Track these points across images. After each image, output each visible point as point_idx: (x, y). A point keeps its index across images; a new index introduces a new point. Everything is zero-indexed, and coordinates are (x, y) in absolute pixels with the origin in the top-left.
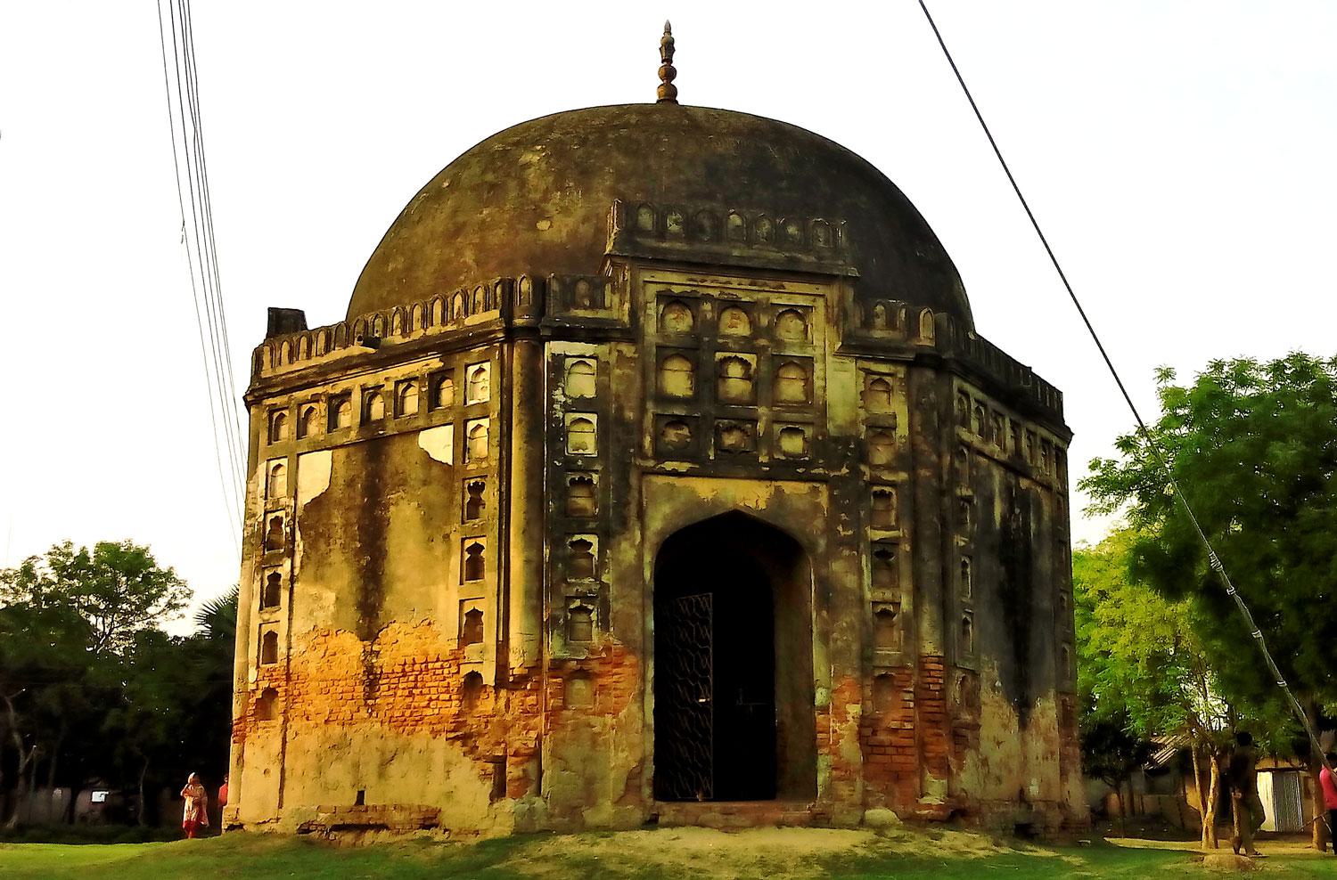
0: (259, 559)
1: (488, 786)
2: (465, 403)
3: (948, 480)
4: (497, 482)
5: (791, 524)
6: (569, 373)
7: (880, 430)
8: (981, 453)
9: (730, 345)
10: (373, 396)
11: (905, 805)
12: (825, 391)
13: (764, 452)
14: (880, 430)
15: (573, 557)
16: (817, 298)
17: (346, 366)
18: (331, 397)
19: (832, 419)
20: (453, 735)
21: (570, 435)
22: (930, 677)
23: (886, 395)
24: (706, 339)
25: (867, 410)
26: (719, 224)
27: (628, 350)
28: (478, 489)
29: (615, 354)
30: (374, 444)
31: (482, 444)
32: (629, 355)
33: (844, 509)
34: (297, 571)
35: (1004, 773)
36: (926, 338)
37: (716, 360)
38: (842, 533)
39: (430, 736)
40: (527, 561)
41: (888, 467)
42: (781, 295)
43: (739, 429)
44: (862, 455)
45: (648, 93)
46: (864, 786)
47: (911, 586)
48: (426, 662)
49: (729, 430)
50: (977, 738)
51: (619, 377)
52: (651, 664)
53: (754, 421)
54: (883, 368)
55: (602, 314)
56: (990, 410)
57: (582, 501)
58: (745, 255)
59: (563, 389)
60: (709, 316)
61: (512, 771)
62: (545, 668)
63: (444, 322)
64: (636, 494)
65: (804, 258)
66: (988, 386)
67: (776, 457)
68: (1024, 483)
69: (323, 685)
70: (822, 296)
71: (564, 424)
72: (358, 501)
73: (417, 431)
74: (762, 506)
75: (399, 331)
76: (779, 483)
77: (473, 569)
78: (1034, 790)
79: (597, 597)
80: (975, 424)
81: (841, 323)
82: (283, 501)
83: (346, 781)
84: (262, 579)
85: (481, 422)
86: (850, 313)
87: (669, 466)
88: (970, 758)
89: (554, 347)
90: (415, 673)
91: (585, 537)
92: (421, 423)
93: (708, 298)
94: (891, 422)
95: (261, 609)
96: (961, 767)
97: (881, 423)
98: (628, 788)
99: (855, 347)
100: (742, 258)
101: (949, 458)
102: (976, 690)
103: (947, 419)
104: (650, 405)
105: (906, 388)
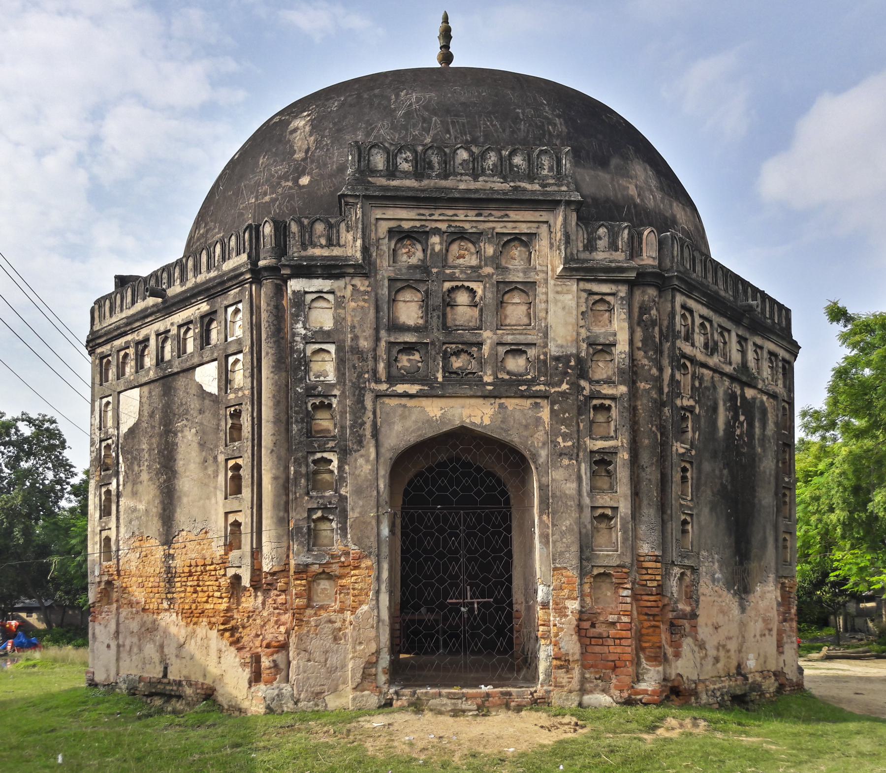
0: (98, 478)
1: (246, 674)
2: (226, 340)
3: (668, 392)
4: (250, 409)
5: (514, 438)
6: (310, 308)
7: (600, 347)
8: (704, 365)
9: (457, 275)
10: (165, 341)
11: (621, 691)
12: (547, 312)
13: (489, 372)
14: (600, 347)
15: (316, 473)
16: (541, 225)
17: (144, 316)
18: (138, 343)
19: (554, 339)
20: (222, 627)
21: (312, 365)
22: (648, 574)
23: (607, 314)
24: (435, 270)
25: (589, 330)
26: (447, 160)
28: (237, 415)
29: (350, 288)
30: (167, 380)
31: (240, 378)
32: (362, 289)
33: (563, 422)
34: (121, 488)
35: (722, 654)
36: (649, 257)
37: (444, 290)
38: (562, 445)
39: (208, 627)
40: (275, 478)
41: (609, 382)
42: (506, 224)
43: (466, 352)
44: (582, 370)
46: (583, 675)
47: (629, 492)
48: (205, 565)
49: (457, 354)
50: (694, 627)
51: (354, 309)
52: (385, 566)
53: (480, 345)
54: (605, 288)
55: (336, 252)
56: (716, 325)
57: (324, 422)
58: (472, 187)
59: (303, 322)
60: (437, 248)
61: (266, 662)
62: (292, 572)
63: (209, 270)
64: (370, 415)
65: (529, 187)
66: (714, 302)
67: (500, 376)
68: (749, 393)
69: (140, 580)
70: (547, 222)
71: (305, 354)
72: (157, 430)
73: (193, 368)
74: (487, 421)
75: (178, 281)
76: (503, 401)
77: (235, 487)
78: (751, 663)
79: (336, 508)
80: (699, 339)
81: (563, 247)
82: (111, 431)
83: (156, 658)
84: (100, 495)
86: (573, 237)
87: (400, 388)
88: (687, 644)
89: (295, 285)
90: (199, 571)
91: (325, 455)
92: (196, 360)
93: (437, 231)
94: (611, 339)
95: (100, 518)
96: (677, 655)
97: (602, 340)
98: (365, 676)
99: (577, 270)
101: (670, 371)
102: (695, 583)
103: (670, 334)
104: (383, 333)
105: (626, 307)
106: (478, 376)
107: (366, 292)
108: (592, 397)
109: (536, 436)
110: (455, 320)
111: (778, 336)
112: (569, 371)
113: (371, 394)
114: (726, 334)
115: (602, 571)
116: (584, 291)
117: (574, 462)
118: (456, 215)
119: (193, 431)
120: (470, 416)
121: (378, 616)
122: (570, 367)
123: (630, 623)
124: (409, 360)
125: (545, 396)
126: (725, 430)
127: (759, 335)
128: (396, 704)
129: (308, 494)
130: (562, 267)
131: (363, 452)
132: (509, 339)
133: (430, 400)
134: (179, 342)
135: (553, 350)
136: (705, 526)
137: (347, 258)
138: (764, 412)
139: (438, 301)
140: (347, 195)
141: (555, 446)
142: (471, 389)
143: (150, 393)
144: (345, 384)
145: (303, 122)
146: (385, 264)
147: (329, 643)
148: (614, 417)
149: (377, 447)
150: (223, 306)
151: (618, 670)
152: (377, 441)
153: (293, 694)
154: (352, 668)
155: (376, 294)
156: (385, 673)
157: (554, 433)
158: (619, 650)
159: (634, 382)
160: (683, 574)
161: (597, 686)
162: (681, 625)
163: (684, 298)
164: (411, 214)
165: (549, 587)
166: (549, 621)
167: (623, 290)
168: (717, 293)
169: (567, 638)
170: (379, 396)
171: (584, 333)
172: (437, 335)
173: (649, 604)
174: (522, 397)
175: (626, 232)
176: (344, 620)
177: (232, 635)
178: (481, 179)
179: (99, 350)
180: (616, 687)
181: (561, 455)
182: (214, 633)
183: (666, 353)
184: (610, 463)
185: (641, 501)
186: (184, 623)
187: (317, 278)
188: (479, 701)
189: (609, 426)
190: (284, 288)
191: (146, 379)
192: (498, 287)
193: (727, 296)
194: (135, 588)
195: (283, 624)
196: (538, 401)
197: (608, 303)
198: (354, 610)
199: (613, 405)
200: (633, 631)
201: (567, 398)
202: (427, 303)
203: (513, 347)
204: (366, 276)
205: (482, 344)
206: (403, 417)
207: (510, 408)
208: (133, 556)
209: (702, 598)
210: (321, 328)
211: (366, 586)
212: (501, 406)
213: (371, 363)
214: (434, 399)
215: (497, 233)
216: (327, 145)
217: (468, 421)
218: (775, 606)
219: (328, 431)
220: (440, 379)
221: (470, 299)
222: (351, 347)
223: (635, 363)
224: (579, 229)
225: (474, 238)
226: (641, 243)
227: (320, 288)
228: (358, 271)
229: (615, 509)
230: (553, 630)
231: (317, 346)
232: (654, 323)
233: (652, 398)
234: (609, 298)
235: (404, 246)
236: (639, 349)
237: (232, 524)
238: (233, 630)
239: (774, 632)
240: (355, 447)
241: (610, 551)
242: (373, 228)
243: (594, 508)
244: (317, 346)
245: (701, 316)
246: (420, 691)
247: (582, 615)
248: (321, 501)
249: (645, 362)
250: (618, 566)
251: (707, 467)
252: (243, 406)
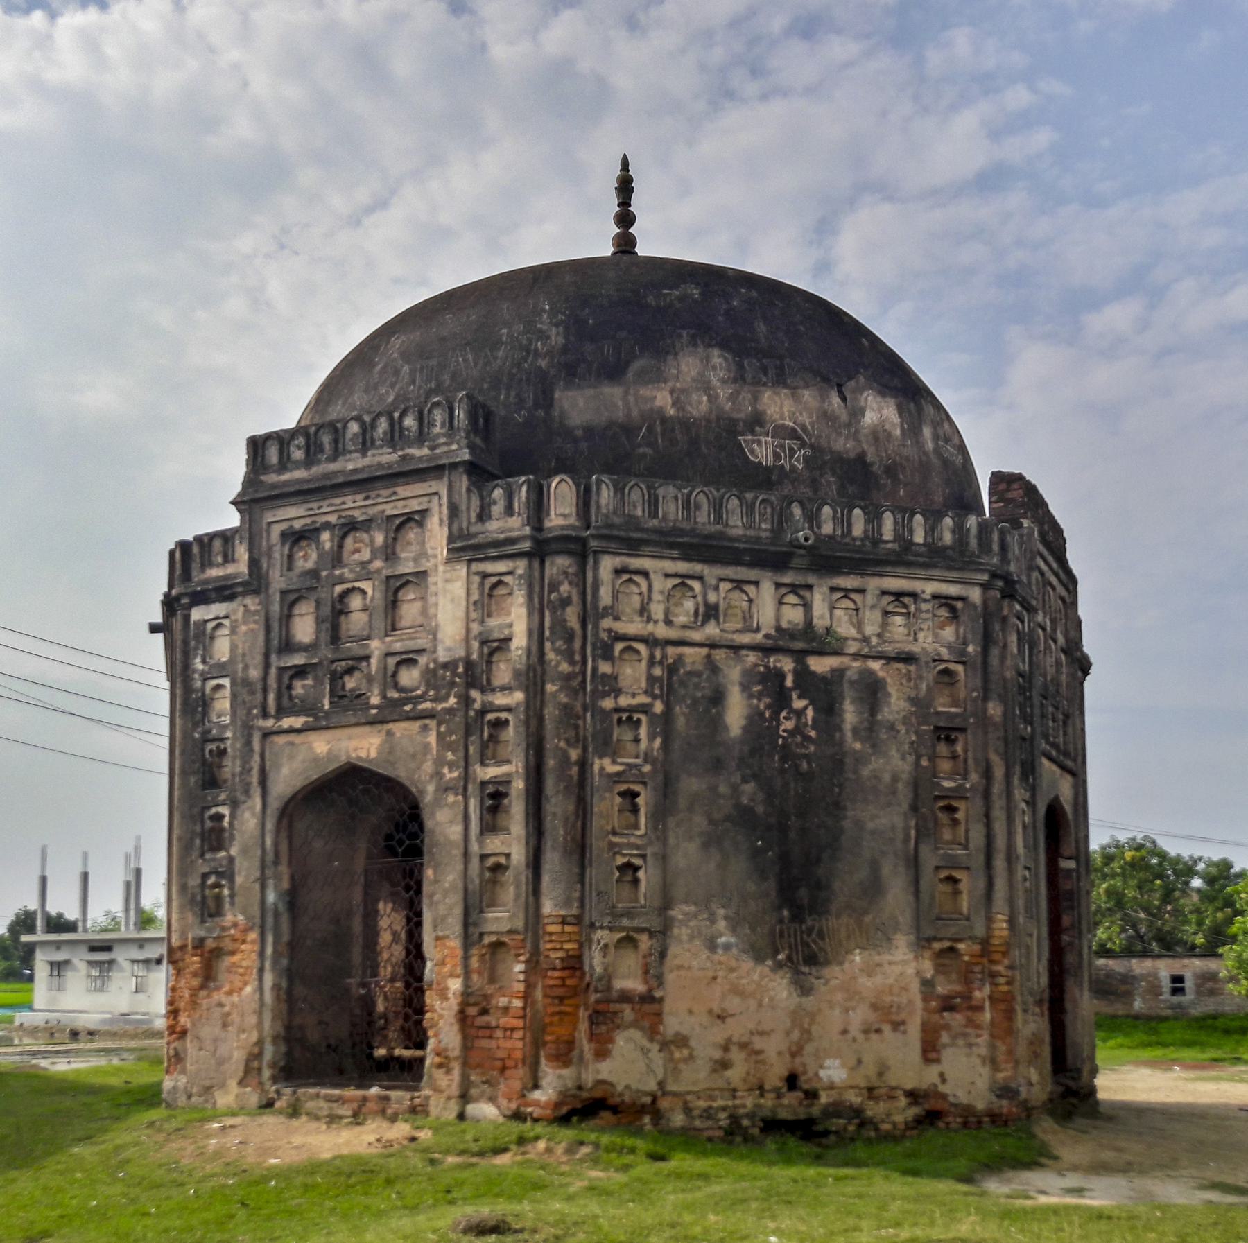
5: (401, 773)
7: (495, 644)
11: (510, 1100)
13: (376, 692)
14: (495, 644)
19: (443, 642)
22: (551, 941)
27: (252, 602)
29: (242, 609)
32: (253, 608)
33: (450, 747)
38: (448, 776)
45: (599, 243)
51: (245, 634)
52: (270, 939)
54: (501, 567)
70: (436, 493)
74: (373, 754)
76: (391, 726)
85: (221, 681)
87: (287, 722)
89: (197, 614)
93: (327, 526)
94: (507, 632)
98: (247, 1071)
100: (355, 471)
104: (274, 658)
107: (257, 611)
108: (483, 712)
110: (348, 630)
112: (457, 680)
115: (494, 938)
116: (477, 573)
118: (344, 503)
122: (458, 676)
124: (304, 686)
125: (430, 715)
128: (278, 1104)
132: (398, 646)
133: (318, 732)
135: (442, 656)
137: (235, 576)
142: (354, 715)
146: (278, 574)
147: (217, 1030)
151: (508, 1072)
157: (440, 762)
158: (509, 1044)
169: (446, 1029)
170: (267, 735)
171: (476, 628)
172: (326, 652)
174: (408, 719)
175: (524, 489)
178: (370, 453)
181: (446, 789)
187: (214, 602)
188: (355, 1105)
204: (256, 592)
207: (398, 735)
220: (327, 707)
225: (366, 525)
229: (508, 856)
234: (507, 579)
235: (301, 549)
243: (483, 857)
246: (301, 1090)
247: (467, 997)
248: (213, 864)
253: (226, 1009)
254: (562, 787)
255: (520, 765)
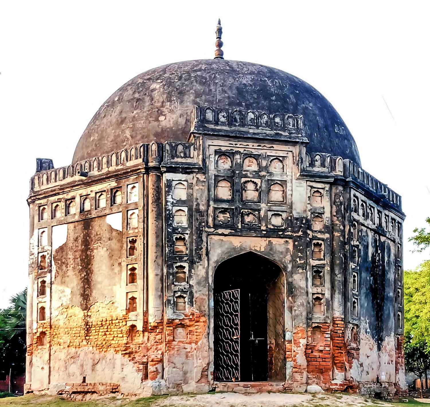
0: (36, 274)
1: (140, 375)
3: (348, 238)
4: (142, 239)
5: (276, 258)
7: (317, 214)
8: (363, 225)
12: (292, 196)
13: (264, 224)
14: (317, 214)
15: (177, 273)
17: (73, 186)
19: (295, 209)
20: (124, 352)
22: (338, 327)
24: (237, 172)
25: (311, 205)
26: (243, 117)
28: (133, 242)
29: (195, 179)
30: (86, 222)
31: (135, 221)
32: (202, 180)
33: (300, 251)
36: (339, 171)
37: (242, 182)
38: (299, 262)
43: (252, 214)
49: (248, 215)
50: (358, 354)
53: (259, 210)
55: (189, 160)
56: (368, 205)
57: (180, 247)
58: (256, 132)
60: (239, 161)
63: (117, 165)
66: (368, 194)
67: (269, 227)
68: (383, 239)
70: (292, 151)
72: (80, 248)
73: (105, 215)
74: (263, 250)
75: (96, 169)
76: (270, 239)
77: (132, 278)
78: (383, 378)
80: (361, 212)
81: (300, 164)
82: (46, 248)
83: (78, 372)
86: (304, 159)
87: (220, 231)
88: (355, 362)
89: (167, 176)
90: (107, 325)
91: (182, 264)
93: (238, 152)
96: (350, 367)
97: (318, 211)
101: (349, 227)
103: (348, 208)
104: (211, 203)
106: (258, 226)
109: (286, 257)
110: (247, 197)
111: (396, 210)
112: (303, 225)
113: (205, 234)
114: (372, 209)
115: (316, 325)
117: (305, 271)
118: (248, 145)
119: (105, 249)
120: (254, 246)
121: (209, 346)
122: (303, 224)
123: (330, 351)
126: (372, 257)
127: (387, 210)
129: (173, 284)
130: (299, 174)
131: (201, 263)
134: (96, 201)
136: (363, 304)
137: (194, 164)
138: (389, 250)
139: (239, 188)
140: (195, 133)
141: (296, 263)
142: (255, 232)
143: (75, 227)
144: (192, 228)
145: (158, 86)
147: (183, 359)
148: (323, 249)
149: (208, 260)
150: (126, 184)
152: (208, 258)
153: (166, 385)
154: (195, 373)
155: (208, 183)
156: (211, 374)
159: (332, 233)
160: (353, 328)
161: (314, 381)
162: (351, 354)
163: (354, 191)
164: (226, 143)
165: (293, 332)
166: (292, 349)
167: (327, 187)
168: (368, 188)
171: (309, 207)
173: (338, 341)
175: (329, 158)
176: (192, 348)
177: (129, 357)
178: (260, 128)
179: (38, 202)
180: (323, 382)
181: (298, 267)
182: (119, 355)
183: (347, 218)
184: (321, 272)
185: (335, 291)
186: (98, 351)
189: (320, 254)
190: (161, 177)
191: (73, 220)
192: (268, 182)
193: (372, 190)
194: (62, 335)
195: (160, 350)
196: (287, 240)
197: (321, 193)
198: (196, 343)
199: (323, 243)
200: (331, 354)
201: (302, 239)
202: (233, 188)
203: (276, 212)
204: (204, 174)
205: (260, 210)
206: (221, 246)
208: (62, 318)
209: (361, 341)
210: (180, 199)
211: (203, 331)
212: (269, 241)
213: (205, 218)
214: (237, 237)
215: (268, 155)
216: (174, 100)
217: (253, 249)
218: (394, 349)
219: (182, 252)
220: (240, 227)
221: (254, 187)
222: (196, 209)
223: (333, 223)
224: (307, 156)
226: (335, 164)
227: (180, 179)
228: (200, 171)
230: (293, 354)
231: (179, 208)
232: (341, 203)
233: (340, 240)
236: (335, 216)
237: (130, 299)
238: (130, 354)
239: (394, 362)
240: (197, 260)
241: (319, 316)
242: (207, 149)
244: (179, 208)
245: (362, 201)
249: (337, 222)
250: (324, 323)
251: (364, 275)
252: (138, 237)
253: (188, 350)
254: (342, 271)
255: (328, 261)
